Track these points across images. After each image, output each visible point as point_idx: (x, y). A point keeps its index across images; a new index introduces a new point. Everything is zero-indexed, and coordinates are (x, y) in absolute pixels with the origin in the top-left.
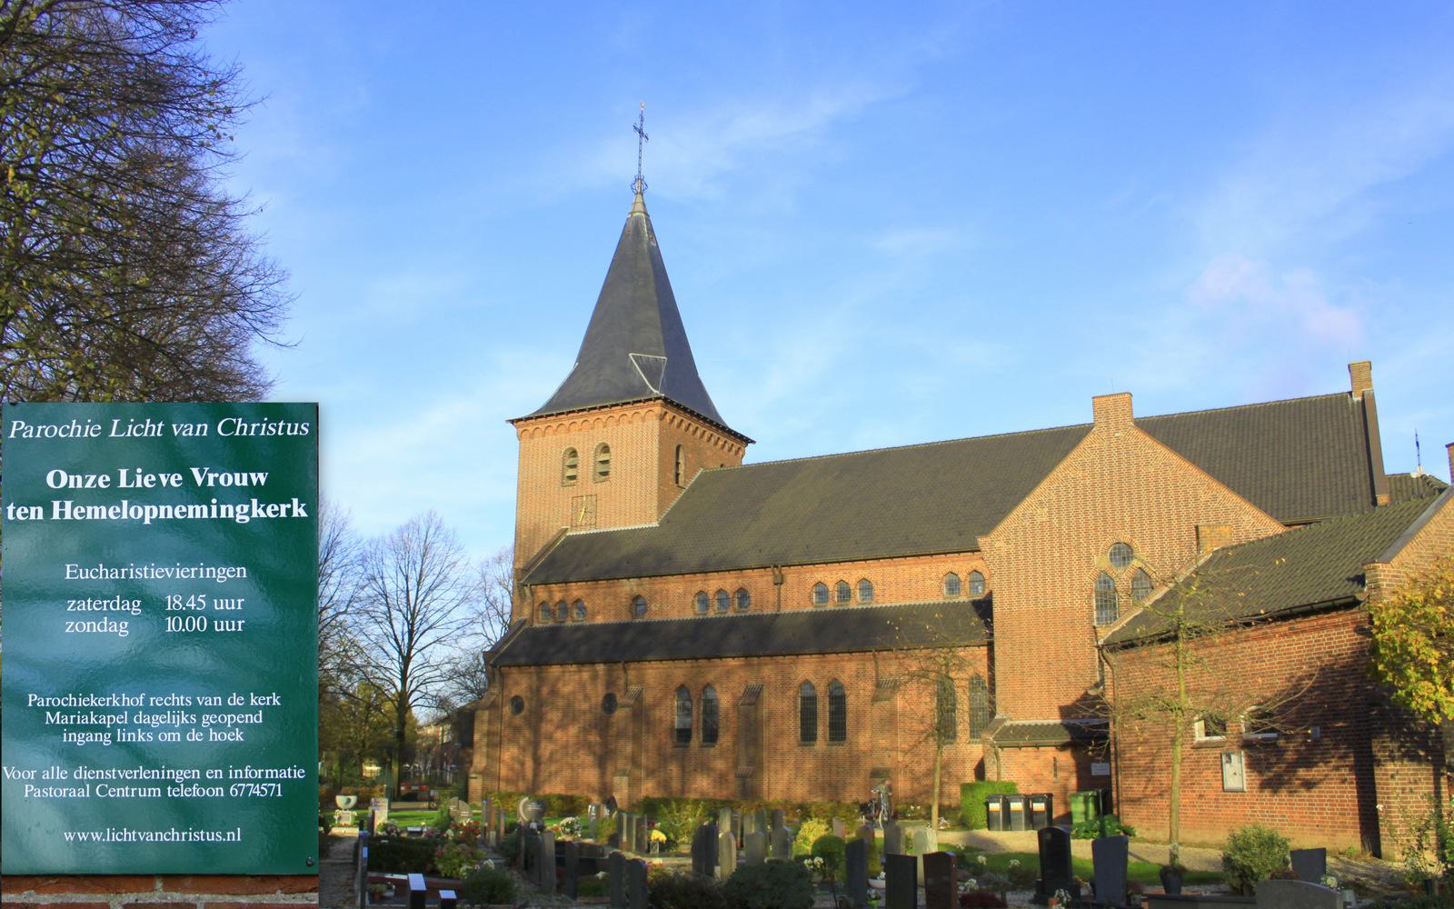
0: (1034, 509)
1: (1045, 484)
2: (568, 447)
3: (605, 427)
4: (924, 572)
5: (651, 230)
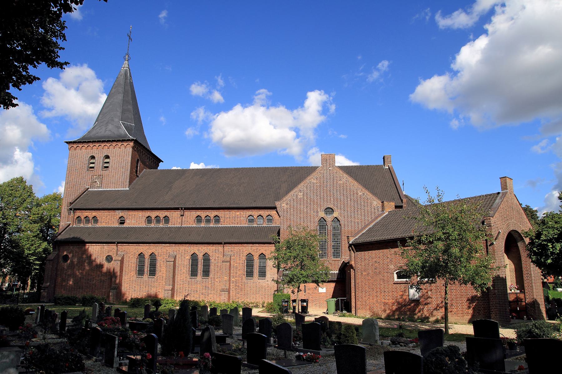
0: (298, 192)
1: (302, 184)
2: (106, 154)
3: (108, 148)
4: (241, 214)
5: (130, 76)
